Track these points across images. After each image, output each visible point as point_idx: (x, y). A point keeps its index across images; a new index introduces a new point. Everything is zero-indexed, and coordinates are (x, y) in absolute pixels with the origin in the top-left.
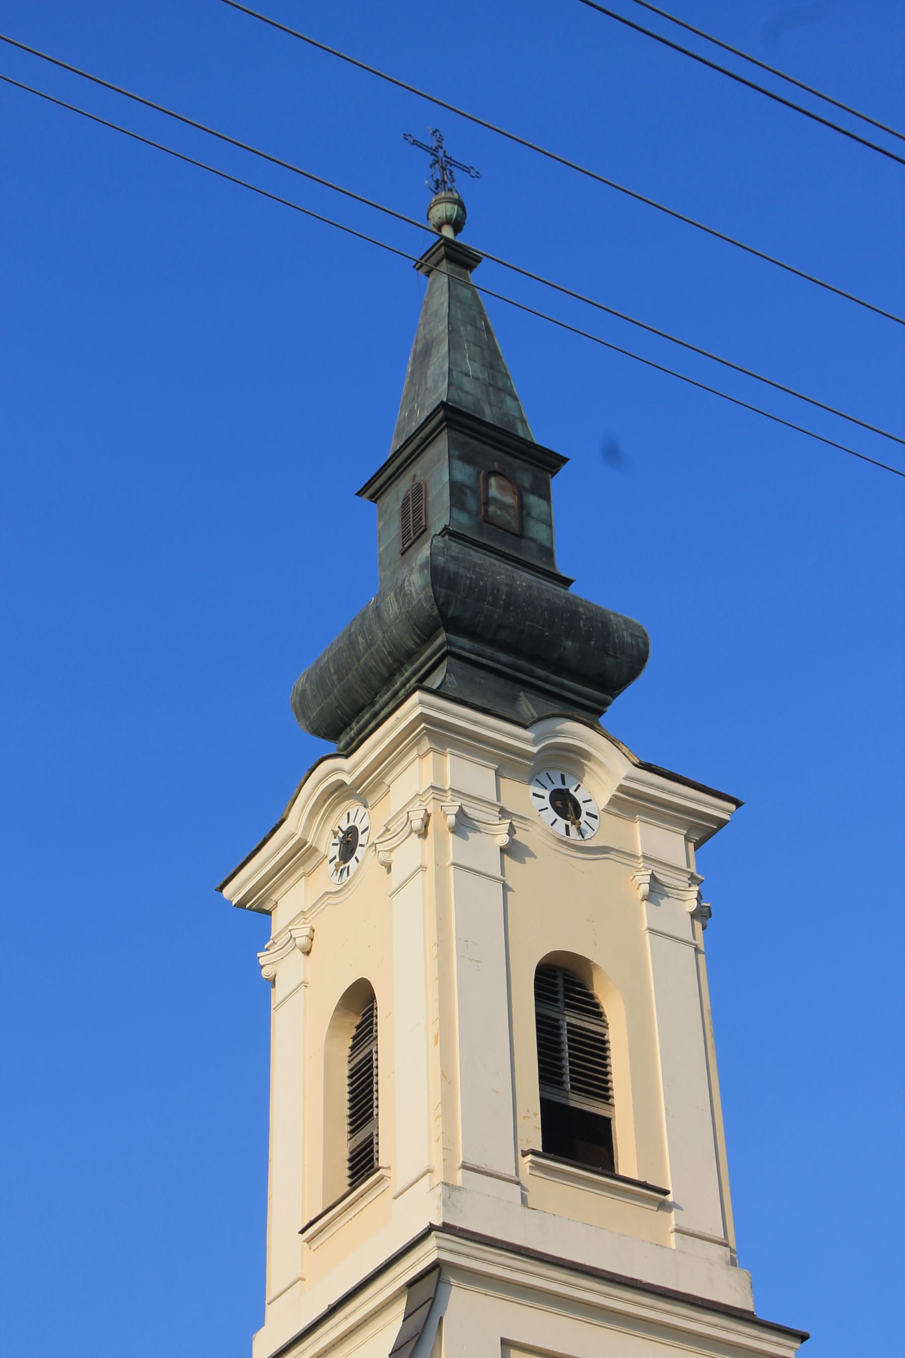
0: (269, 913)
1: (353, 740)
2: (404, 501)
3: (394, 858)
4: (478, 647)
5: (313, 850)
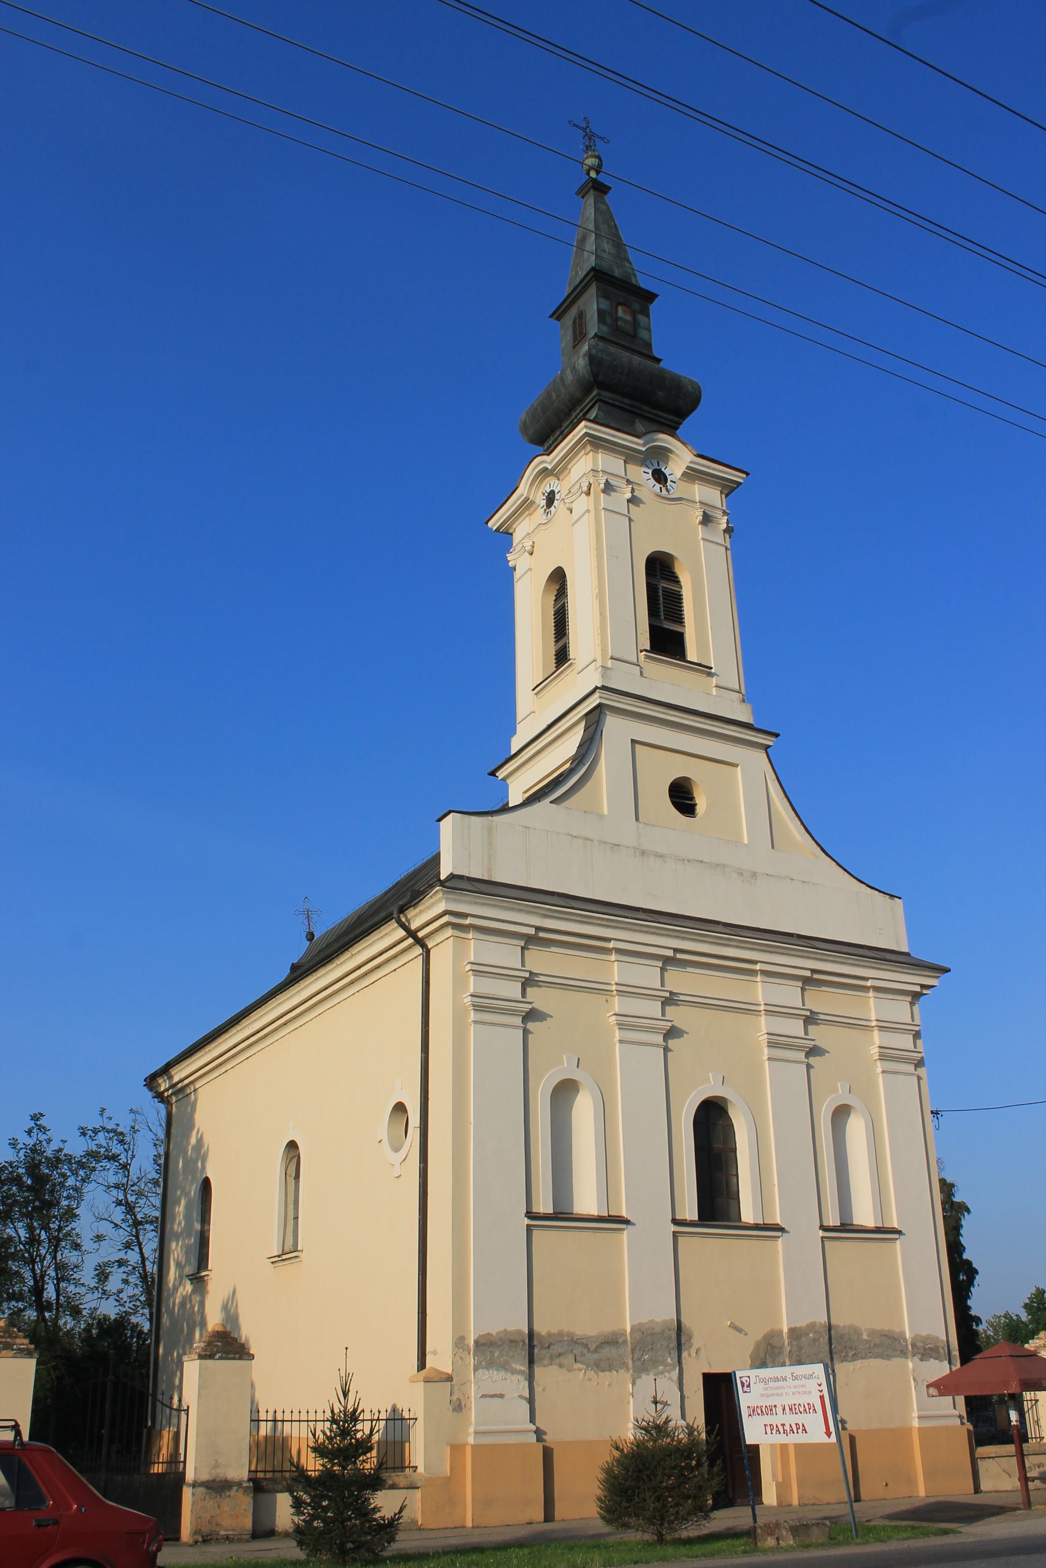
0: (512, 534)
2: (237, 1305)
3: (574, 506)
5: (533, 503)
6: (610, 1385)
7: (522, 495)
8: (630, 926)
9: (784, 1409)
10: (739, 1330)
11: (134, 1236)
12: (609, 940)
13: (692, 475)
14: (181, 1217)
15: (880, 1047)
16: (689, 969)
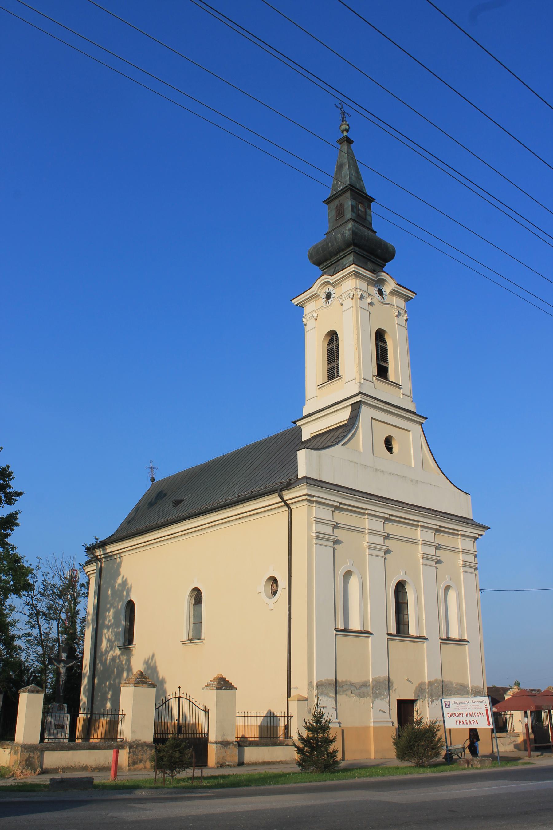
0: (304, 308)
1: (324, 267)
3: (343, 303)
4: (360, 250)
5: (318, 296)
6: (364, 703)
7: (314, 291)
8: (374, 504)
9: (467, 715)
10: (410, 681)
11: (37, 622)
12: (366, 509)
13: (394, 293)
14: (111, 618)
15: (463, 561)
16: (393, 523)
